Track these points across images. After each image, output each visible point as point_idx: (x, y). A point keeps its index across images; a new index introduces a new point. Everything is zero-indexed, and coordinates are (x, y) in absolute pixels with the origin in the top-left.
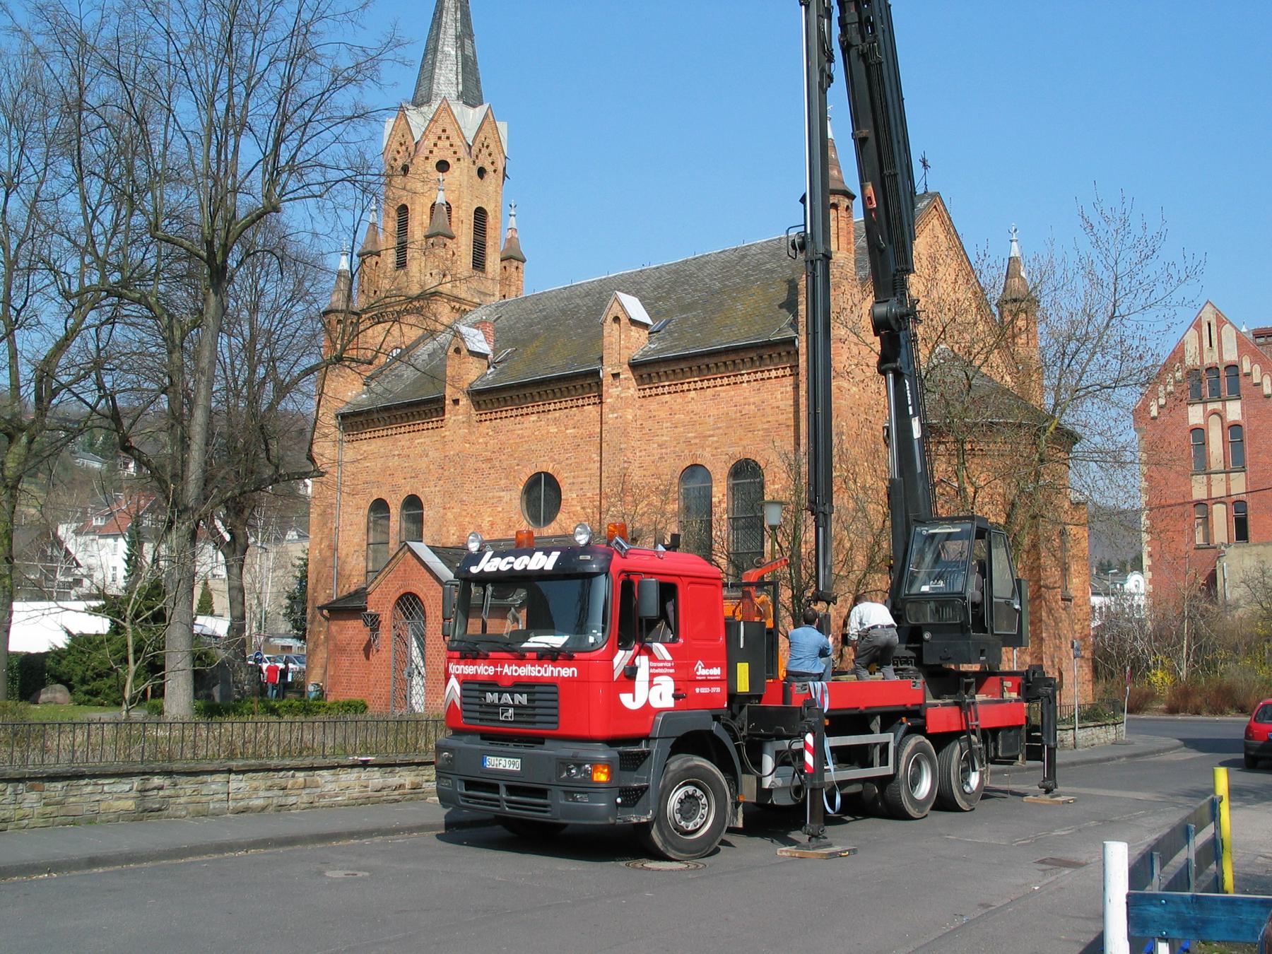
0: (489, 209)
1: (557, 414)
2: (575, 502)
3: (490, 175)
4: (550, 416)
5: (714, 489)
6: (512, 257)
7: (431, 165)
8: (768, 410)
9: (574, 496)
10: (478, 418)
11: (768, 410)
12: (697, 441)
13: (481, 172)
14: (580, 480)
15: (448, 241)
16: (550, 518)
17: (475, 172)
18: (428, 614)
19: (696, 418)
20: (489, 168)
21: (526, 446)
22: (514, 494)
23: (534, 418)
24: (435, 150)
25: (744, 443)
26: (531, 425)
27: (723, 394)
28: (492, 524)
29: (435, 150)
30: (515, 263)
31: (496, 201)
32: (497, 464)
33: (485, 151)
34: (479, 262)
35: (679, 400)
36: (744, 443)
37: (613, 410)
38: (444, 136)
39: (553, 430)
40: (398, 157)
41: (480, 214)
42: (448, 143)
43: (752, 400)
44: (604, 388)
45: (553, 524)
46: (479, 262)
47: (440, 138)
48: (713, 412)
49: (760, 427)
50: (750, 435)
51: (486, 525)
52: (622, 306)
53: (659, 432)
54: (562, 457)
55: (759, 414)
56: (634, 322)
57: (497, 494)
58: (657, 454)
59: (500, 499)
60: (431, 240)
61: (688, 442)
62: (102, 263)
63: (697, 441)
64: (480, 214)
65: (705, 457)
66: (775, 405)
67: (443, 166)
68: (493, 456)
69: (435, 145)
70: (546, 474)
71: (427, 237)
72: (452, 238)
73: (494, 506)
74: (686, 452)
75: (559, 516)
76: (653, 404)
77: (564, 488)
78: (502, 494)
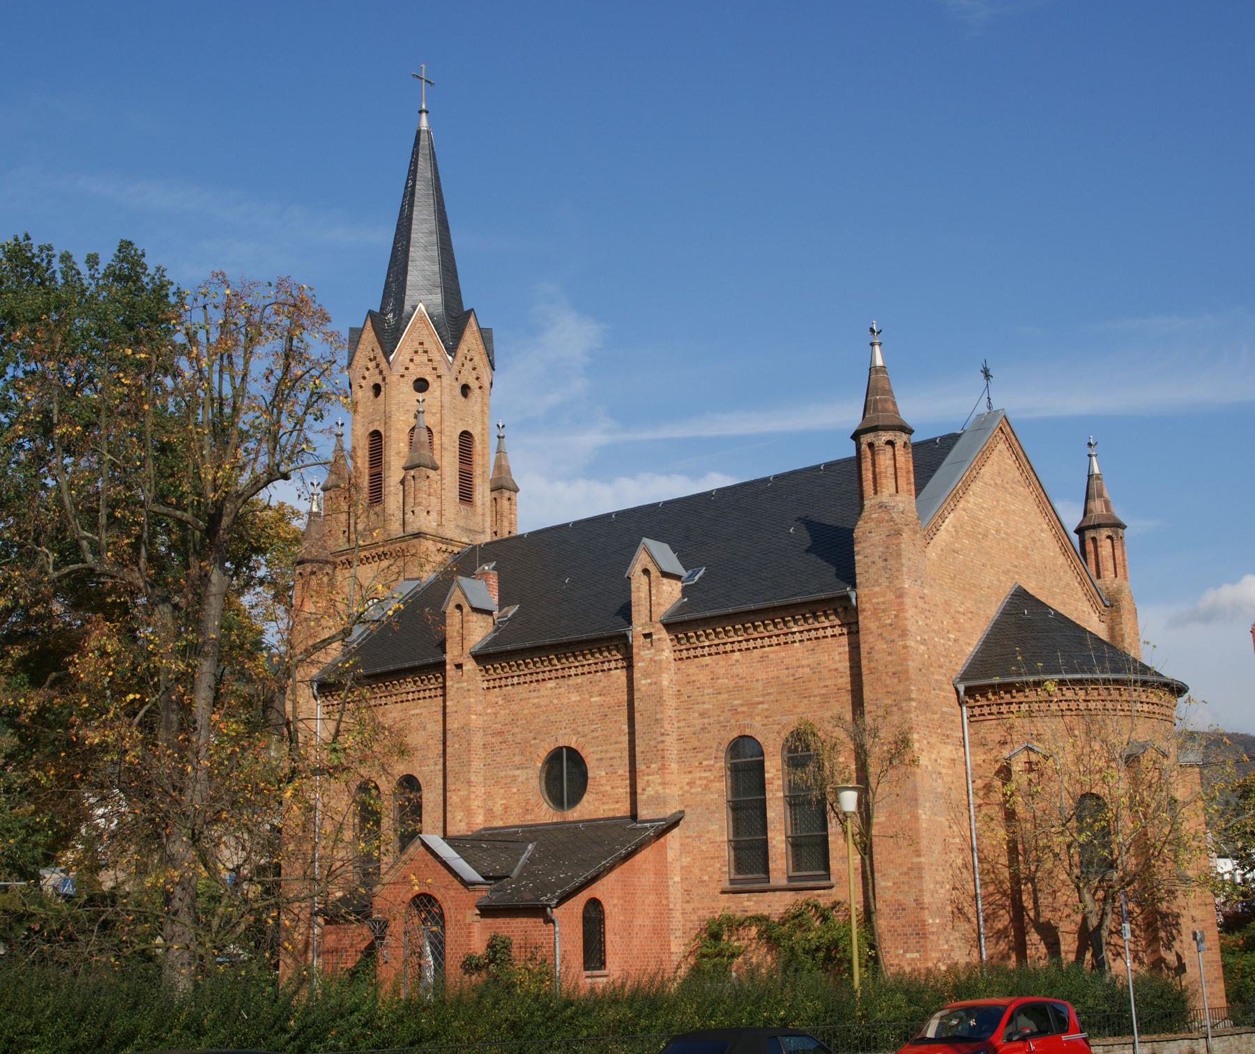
0: (476, 432)
1: (579, 680)
2: (604, 781)
3: (475, 393)
4: (571, 681)
5: (767, 764)
6: (503, 487)
7: (407, 387)
8: (826, 674)
9: (603, 773)
10: (485, 685)
11: (826, 674)
12: (745, 709)
13: (465, 390)
14: (611, 755)
15: (431, 473)
16: (575, 799)
17: (458, 391)
18: (447, 917)
19: (742, 683)
20: (474, 385)
21: (543, 717)
22: (530, 771)
23: (551, 684)
24: (411, 366)
25: (799, 710)
26: (549, 692)
27: (771, 656)
28: (506, 808)
29: (411, 366)
30: (507, 494)
31: (483, 423)
32: (510, 738)
33: (468, 365)
34: (466, 495)
35: (722, 663)
36: (799, 710)
37: (646, 675)
38: (420, 351)
39: (575, 697)
40: (367, 374)
41: (466, 437)
42: (425, 358)
43: (805, 662)
44: (635, 651)
45: (578, 807)
46: (466, 495)
47: (416, 352)
48: (762, 675)
49: (816, 692)
50: (805, 701)
51: (498, 809)
52: (651, 557)
53: (700, 699)
54: (586, 729)
55: (815, 677)
56: (665, 575)
57: (511, 773)
58: (698, 723)
59: (514, 778)
60: (412, 472)
61: (734, 710)
62: (306, 619)
63: (745, 709)
64: (466, 437)
65: (756, 729)
66: (834, 666)
67: (421, 385)
68: (505, 729)
69: (412, 360)
70: (569, 749)
71: (406, 469)
72: (435, 468)
73: (507, 786)
74: (733, 722)
75: (586, 798)
76: (691, 668)
77: (591, 763)
78: (517, 772)
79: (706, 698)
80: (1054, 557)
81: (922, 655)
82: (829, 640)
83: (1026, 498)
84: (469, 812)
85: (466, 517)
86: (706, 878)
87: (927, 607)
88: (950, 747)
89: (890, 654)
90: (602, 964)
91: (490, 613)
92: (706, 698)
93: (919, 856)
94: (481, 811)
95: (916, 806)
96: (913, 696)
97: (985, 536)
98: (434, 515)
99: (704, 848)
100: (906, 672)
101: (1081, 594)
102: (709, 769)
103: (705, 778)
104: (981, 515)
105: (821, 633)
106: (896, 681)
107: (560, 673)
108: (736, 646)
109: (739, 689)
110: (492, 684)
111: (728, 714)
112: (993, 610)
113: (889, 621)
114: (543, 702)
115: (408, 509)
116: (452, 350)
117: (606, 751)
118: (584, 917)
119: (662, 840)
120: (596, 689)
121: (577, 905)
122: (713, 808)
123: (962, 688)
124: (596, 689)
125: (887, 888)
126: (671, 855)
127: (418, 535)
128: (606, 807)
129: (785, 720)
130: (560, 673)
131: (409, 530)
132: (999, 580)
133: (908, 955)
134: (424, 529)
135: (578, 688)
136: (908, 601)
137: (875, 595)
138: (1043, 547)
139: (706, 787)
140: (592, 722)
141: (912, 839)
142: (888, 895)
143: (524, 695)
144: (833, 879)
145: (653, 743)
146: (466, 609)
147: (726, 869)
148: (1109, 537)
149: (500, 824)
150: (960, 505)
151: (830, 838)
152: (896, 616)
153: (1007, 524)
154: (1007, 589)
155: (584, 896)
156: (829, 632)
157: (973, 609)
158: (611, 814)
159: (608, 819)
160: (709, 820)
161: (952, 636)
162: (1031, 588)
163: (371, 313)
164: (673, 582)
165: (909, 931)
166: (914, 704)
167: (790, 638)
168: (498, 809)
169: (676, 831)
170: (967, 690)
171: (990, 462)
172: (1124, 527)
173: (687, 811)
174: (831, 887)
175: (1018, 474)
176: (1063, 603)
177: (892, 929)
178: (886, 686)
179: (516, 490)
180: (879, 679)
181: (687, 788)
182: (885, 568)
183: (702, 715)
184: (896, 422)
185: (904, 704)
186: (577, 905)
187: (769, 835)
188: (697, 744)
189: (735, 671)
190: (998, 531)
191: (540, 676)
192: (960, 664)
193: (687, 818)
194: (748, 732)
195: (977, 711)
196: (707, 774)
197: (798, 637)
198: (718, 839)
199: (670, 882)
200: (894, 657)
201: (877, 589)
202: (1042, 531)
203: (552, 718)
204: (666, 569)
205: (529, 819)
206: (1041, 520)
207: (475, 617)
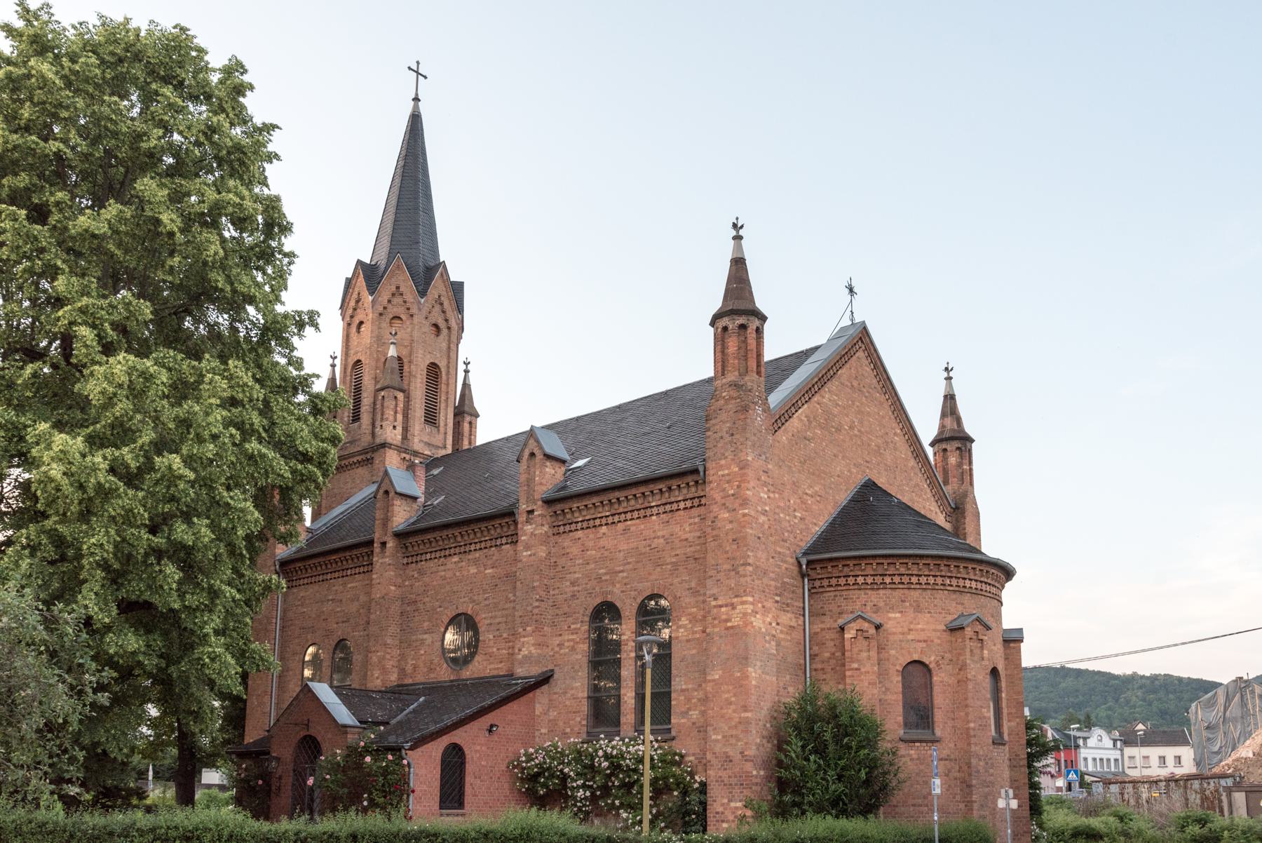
10: (405, 561)
12: (608, 577)
14: (497, 620)
19: (606, 553)
21: (448, 588)
23: (456, 559)
25: (653, 577)
26: (453, 566)
27: (633, 529)
29: (390, 306)
32: (421, 606)
35: (591, 536)
36: (653, 577)
39: (473, 570)
43: (660, 534)
45: (471, 666)
48: (624, 547)
50: (658, 569)
56: (549, 457)
61: (599, 579)
63: (608, 577)
66: (684, 537)
78: (425, 636)
79: (577, 569)
80: (907, 460)
81: (762, 525)
82: (681, 513)
83: (881, 403)
84: (384, 671)
85: (430, 434)
86: (568, 730)
87: (770, 481)
88: (789, 615)
89: (731, 522)
90: (460, 804)
91: (415, 499)
92: (577, 569)
93: (746, 711)
94: (396, 670)
95: (747, 665)
96: (750, 561)
97: (838, 430)
98: (399, 429)
99: (568, 703)
100: (745, 538)
101: (929, 495)
102: (575, 632)
103: (572, 640)
104: (835, 411)
105: (675, 506)
106: (735, 547)
107: (462, 550)
108: (604, 521)
109: (603, 558)
110: (410, 560)
111: (594, 582)
112: (843, 497)
113: (731, 492)
114: (449, 574)
115: (378, 423)
116: (423, 293)
117: (496, 617)
118: (443, 761)
119: (531, 695)
120: (490, 562)
121: (435, 750)
122: (577, 667)
123: (804, 561)
124: (490, 562)
125: (717, 741)
126: (539, 709)
127: (384, 445)
128: (492, 666)
129: (640, 586)
130: (462, 550)
131: (378, 441)
132: (849, 471)
133: (733, 804)
134: (389, 440)
135: (476, 561)
136: (750, 473)
137: (721, 467)
138: (895, 449)
139: (573, 649)
140: (485, 591)
141: (1012, 767)
142: (718, 748)
143: (434, 569)
144: (673, 733)
145: (529, 608)
146: (392, 494)
147: (584, 722)
148: (958, 448)
149: (410, 681)
150: (815, 399)
151: (673, 695)
152: (739, 487)
153: (861, 422)
154: (858, 480)
155: (445, 741)
156: (682, 505)
157: (823, 493)
158: (495, 673)
159: (494, 677)
160: (573, 678)
161: (798, 514)
162: (882, 482)
163: (359, 263)
164: (557, 465)
165: (734, 781)
166: (750, 569)
167: (648, 512)
168: (409, 669)
169: (545, 688)
170: (809, 563)
171: (847, 366)
172: (973, 441)
173: (556, 669)
174: (673, 739)
175: (875, 381)
176: (911, 500)
177: (720, 780)
178: (727, 552)
179: (477, 416)
180: (720, 546)
181: (557, 649)
182: (731, 442)
183: (573, 584)
184: (750, 307)
185: (741, 569)
186: (435, 750)
187: (622, 692)
188: (566, 609)
189: (602, 542)
190: (851, 428)
191: (447, 552)
192: (807, 540)
193: (556, 676)
194: (610, 598)
195: (817, 583)
196: (574, 637)
197: (655, 510)
198: (580, 695)
199: (537, 733)
200: (735, 525)
201: (723, 462)
202: (895, 434)
203: (455, 589)
204: (549, 451)
205: (432, 677)
206: (895, 425)
207: (398, 502)
